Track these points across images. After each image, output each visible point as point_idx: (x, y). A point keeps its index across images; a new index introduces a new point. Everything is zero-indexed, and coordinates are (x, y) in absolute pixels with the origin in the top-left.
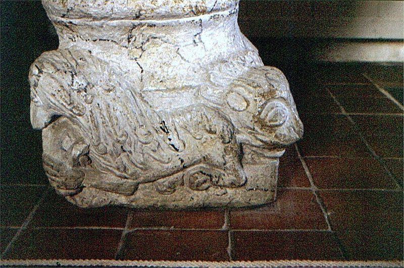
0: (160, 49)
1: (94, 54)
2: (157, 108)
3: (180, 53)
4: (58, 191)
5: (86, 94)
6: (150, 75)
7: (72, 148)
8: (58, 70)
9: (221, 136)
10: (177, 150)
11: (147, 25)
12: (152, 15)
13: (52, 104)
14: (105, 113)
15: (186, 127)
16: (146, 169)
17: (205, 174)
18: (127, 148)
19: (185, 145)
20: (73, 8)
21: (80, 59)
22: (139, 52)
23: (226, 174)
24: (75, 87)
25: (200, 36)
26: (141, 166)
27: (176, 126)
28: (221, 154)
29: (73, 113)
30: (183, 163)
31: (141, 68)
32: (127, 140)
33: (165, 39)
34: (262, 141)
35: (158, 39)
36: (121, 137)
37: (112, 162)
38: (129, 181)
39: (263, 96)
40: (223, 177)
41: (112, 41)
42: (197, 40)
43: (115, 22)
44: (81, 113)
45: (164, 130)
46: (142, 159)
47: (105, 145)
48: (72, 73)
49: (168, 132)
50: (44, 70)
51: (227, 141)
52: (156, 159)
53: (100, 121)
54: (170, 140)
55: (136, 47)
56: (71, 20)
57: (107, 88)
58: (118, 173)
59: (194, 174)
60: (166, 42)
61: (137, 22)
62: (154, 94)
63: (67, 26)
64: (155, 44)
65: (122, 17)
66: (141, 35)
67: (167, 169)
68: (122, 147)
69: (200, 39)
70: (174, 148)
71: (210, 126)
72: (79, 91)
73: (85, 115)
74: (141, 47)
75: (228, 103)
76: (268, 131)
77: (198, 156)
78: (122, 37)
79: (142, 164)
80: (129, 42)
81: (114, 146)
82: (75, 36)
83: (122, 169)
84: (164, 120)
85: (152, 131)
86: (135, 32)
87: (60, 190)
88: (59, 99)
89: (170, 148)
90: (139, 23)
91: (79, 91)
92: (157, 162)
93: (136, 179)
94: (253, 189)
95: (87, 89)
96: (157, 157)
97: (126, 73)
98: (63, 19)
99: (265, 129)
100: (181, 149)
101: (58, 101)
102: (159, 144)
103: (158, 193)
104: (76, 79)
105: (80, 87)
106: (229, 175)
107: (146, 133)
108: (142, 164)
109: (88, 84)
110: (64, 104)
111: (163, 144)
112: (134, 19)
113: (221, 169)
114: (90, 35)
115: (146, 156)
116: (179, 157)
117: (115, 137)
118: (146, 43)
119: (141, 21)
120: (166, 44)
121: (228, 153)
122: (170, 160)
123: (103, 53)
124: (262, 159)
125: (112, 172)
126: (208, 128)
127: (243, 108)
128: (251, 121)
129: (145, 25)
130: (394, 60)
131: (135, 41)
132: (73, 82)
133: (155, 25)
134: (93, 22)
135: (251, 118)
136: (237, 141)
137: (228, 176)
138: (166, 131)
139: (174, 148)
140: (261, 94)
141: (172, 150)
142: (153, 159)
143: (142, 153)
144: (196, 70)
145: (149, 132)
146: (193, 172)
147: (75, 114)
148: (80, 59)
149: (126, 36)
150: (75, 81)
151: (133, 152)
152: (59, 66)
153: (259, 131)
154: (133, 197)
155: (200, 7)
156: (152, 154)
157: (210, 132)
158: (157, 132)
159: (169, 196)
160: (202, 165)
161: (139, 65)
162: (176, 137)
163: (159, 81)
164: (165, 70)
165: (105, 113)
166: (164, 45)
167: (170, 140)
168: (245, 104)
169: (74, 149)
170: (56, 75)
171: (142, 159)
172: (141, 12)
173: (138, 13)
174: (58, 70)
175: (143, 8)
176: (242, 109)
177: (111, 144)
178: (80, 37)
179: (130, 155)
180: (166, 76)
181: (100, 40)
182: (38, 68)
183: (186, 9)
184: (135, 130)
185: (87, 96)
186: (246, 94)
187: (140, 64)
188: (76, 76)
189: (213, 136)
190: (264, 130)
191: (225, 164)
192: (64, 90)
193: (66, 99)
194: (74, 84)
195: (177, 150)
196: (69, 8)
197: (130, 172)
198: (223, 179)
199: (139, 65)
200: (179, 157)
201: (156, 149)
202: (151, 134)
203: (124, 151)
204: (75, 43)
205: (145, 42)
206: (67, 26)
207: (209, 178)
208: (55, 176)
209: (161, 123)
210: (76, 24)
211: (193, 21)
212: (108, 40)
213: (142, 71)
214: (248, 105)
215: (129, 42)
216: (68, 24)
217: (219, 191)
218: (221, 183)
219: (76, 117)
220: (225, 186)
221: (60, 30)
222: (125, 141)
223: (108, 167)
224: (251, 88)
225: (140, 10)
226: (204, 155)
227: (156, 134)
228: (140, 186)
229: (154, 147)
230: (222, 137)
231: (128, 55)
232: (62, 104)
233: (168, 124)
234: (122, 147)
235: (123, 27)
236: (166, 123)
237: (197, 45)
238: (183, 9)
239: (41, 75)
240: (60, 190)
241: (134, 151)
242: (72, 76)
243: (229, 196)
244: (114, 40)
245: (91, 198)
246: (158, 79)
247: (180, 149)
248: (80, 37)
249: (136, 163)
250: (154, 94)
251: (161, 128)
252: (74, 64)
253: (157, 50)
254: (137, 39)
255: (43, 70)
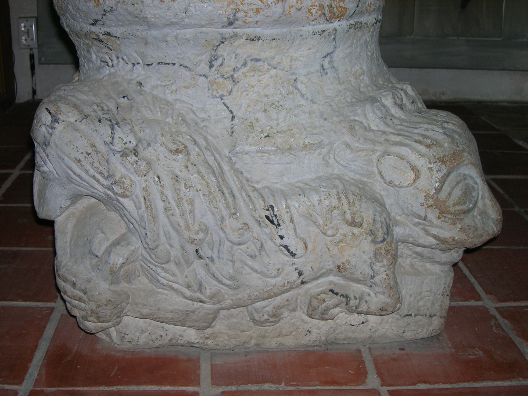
0: (266, 79)
1: (147, 88)
2: (258, 182)
3: (299, 87)
4: (83, 324)
5: (136, 159)
6: (247, 123)
7: (108, 252)
8: (87, 116)
9: (371, 230)
10: (293, 255)
11: (245, 37)
12: (257, 19)
13: (116, 345)
14: (169, 193)
15: (311, 216)
16: (237, 288)
17: (337, 294)
18: (205, 251)
19: (306, 247)
20: (114, 8)
21: (124, 97)
22: (228, 84)
23: (372, 293)
24: (118, 146)
25: (332, 58)
26: (229, 282)
27: (293, 212)
28: (369, 261)
29: (113, 192)
30: (302, 277)
31: (231, 112)
32: (207, 239)
33: (274, 62)
34: (435, 237)
35: (260, 63)
36: (197, 233)
37: (179, 275)
38: (207, 306)
39: (443, 162)
40: (367, 298)
41: (181, 65)
42: (326, 65)
43: (189, 32)
44: (127, 193)
45: (272, 222)
46: (231, 271)
47: (168, 246)
48: (111, 121)
49: (279, 225)
50: (61, 117)
51: (380, 239)
52: (256, 271)
53: (160, 205)
54: (282, 237)
55: (223, 76)
56: (109, 30)
57: (174, 147)
58: (188, 293)
59: (319, 295)
60: (275, 68)
61: (229, 30)
62: (254, 157)
63: (101, 41)
64: (254, 70)
65: (203, 23)
66: (234, 55)
67: (274, 286)
68: (197, 251)
69: (331, 62)
70: (288, 250)
71: (353, 214)
72: (124, 155)
73: (134, 196)
74: (232, 76)
75: (380, 173)
76: (450, 221)
77: (330, 264)
78: (199, 58)
79: (231, 278)
80: (211, 66)
81: (183, 248)
82: (114, 58)
83: (195, 287)
84: (273, 205)
85: (251, 222)
86: (224, 51)
87: (87, 323)
88: (89, 167)
89: (282, 251)
90: (232, 34)
91: (124, 155)
92: (256, 275)
93: (219, 302)
94: (411, 315)
95: (138, 150)
96: (256, 266)
97: (204, 121)
98: (93, 29)
99: (444, 217)
100: (299, 252)
101: (87, 172)
102: (262, 245)
103: (251, 324)
104: (119, 133)
105: (126, 146)
106: (378, 294)
107: (240, 226)
108: (231, 278)
109: (139, 141)
110: (98, 176)
111: (269, 245)
112: (223, 27)
113: (366, 285)
114: (142, 56)
115: (238, 265)
116: (295, 266)
117: (186, 234)
118: (241, 68)
119: (234, 30)
120: (275, 70)
121: (380, 260)
122: (280, 271)
123: (165, 86)
124: (428, 265)
125: (176, 291)
126: (348, 217)
127: (409, 182)
128: (422, 205)
129: (241, 37)
130: (517, 98)
131: (221, 65)
132: (113, 138)
133: (259, 38)
134: (149, 32)
135: (422, 200)
136: (395, 237)
137: (376, 296)
138: (276, 223)
139: (288, 250)
140: (438, 159)
141: (287, 256)
142: (249, 270)
143: (232, 261)
144: (326, 116)
145: (246, 224)
146: (319, 290)
147: (115, 194)
148: (124, 97)
149: (206, 57)
150: (116, 136)
151: (216, 259)
152: (87, 110)
153: (436, 222)
154: (209, 331)
155: (337, 8)
156: (250, 262)
157: (353, 223)
158: (260, 224)
159: (271, 328)
160: (331, 278)
161: (227, 107)
162: (291, 232)
163: (263, 136)
164: (274, 116)
165: (169, 193)
166: (273, 72)
167: (282, 237)
168: (412, 175)
169: (112, 254)
170: (82, 126)
171: (231, 271)
172: (238, 15)
173: (231, 17)
174: (87, 116)
175: (241, 7)
176: (406, 184)
177: (177, 245)
178: (123, 59)
179: (210, 263)
180: (275, 127)
181: (159, 63)
182: (50, 113)
183: (313, 11)
184: (222, 222)
185: (139, 163)
186: (413, 157)
187: (228, 105)
188: (119, 127)
189: (356, 230)
190: (443, 219)
191: (372, 278)
192: (97, 152)
193: (101, 168)
194: (116, 141)
195: (293, 255)
196: (105, 8)
197: (208, 292)
198: (366, 302)
199: (227, 107)
200: (295, 266)
201: (257, 254)
202: (249, 228)
203: (201, 257)
204: (113, 70)
205: (239, 66)
206: (101, 41)
207: (344, 300)
208: (80, 300)
209: (268, 210)
210: (118, 35)
211: (323, 31)
212: (174, 64)
213: (233, 117)
214: (417, 177)
215: (211, 66)
216: (101, 36)
217: (356, 319)
218: (363, 307)
219: (118, 201)
220: (367, 313)
221: (85, 47)
222: (202, 241)
223: (171, 284)
224: (422, 148)
225: (237, 10)
226: (339, 264)
227: (258, 228)
228: (223, 313)
229: (253, 248)
230: (372, 233)
231: (209, 90)
232: (93, 177)
233: (280, 209)
234: (197, 251)
235: (204, 41)
236: (276, 209)
237: (327, 73)
238: (309, 10)
239: (56, 125)
240: (87, 323)
241: (219, 257)
242: (112, 128)
243: (370, 327)
244: (184, 64)
245: (138, 334)
246: (262, 132)
247: (299, 253)
248: (123, 59)
249: (220, 277)
250: (254, 157)
251: (267, 217)
252: (112, 106)
253: (259, 81)
254: (226, 63)
255: (59, 116)
